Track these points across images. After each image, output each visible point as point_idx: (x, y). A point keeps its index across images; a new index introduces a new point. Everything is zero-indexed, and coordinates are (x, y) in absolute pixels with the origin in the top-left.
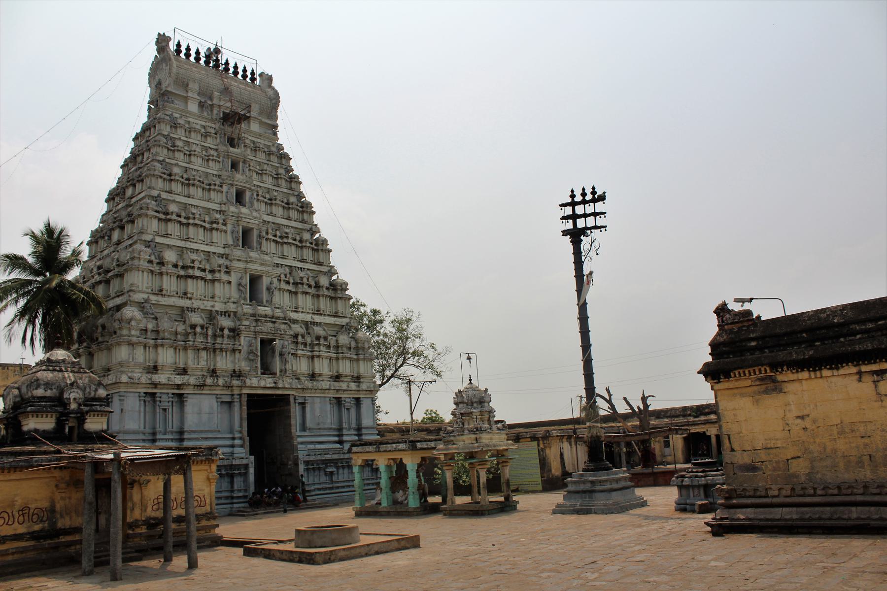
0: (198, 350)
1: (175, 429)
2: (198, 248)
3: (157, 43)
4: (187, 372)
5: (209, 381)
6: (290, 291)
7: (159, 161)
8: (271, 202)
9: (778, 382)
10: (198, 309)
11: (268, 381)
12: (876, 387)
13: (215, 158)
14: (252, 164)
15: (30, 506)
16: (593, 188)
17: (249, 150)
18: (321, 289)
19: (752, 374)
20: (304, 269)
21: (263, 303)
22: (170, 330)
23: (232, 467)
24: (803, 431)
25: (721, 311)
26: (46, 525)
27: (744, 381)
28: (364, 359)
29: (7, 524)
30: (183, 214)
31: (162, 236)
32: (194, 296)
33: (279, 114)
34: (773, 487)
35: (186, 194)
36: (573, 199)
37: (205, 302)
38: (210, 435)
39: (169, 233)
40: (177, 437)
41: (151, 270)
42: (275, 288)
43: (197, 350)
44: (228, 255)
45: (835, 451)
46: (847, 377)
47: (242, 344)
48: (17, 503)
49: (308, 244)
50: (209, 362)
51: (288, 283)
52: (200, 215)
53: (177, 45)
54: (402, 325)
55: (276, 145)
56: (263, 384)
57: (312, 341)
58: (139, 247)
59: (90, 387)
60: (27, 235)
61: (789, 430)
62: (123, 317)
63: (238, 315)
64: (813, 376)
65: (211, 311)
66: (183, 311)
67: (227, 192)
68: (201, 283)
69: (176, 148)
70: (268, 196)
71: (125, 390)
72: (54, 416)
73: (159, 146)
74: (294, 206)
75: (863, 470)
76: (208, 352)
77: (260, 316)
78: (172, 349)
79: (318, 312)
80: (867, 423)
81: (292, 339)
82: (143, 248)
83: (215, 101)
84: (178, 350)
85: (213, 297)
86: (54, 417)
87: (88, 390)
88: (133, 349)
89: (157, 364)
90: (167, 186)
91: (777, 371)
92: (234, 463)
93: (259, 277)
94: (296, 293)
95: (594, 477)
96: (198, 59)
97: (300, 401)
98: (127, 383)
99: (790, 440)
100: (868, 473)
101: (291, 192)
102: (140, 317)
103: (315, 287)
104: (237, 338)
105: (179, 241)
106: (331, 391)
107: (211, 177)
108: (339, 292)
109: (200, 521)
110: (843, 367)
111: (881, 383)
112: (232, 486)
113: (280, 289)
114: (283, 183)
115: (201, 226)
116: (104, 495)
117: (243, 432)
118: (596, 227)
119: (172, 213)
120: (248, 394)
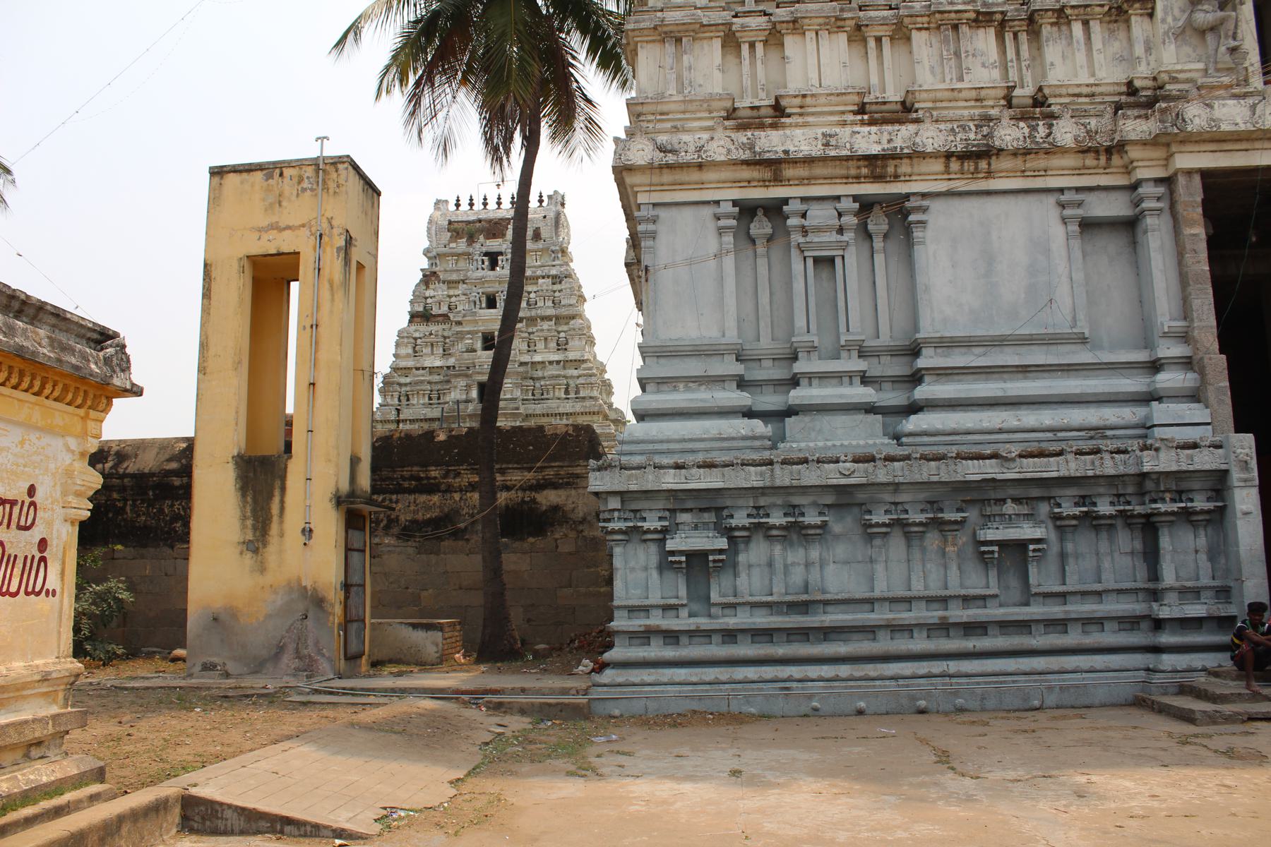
0: (955, 27)
1: (885, 339)
5: (1009, 134)
71: (656, 198)
76: (1009, 37)
84: (872, 43)
92: (1147, 468)
98: (650, 167)
112: (1154, 575)
120: (1206, 174)
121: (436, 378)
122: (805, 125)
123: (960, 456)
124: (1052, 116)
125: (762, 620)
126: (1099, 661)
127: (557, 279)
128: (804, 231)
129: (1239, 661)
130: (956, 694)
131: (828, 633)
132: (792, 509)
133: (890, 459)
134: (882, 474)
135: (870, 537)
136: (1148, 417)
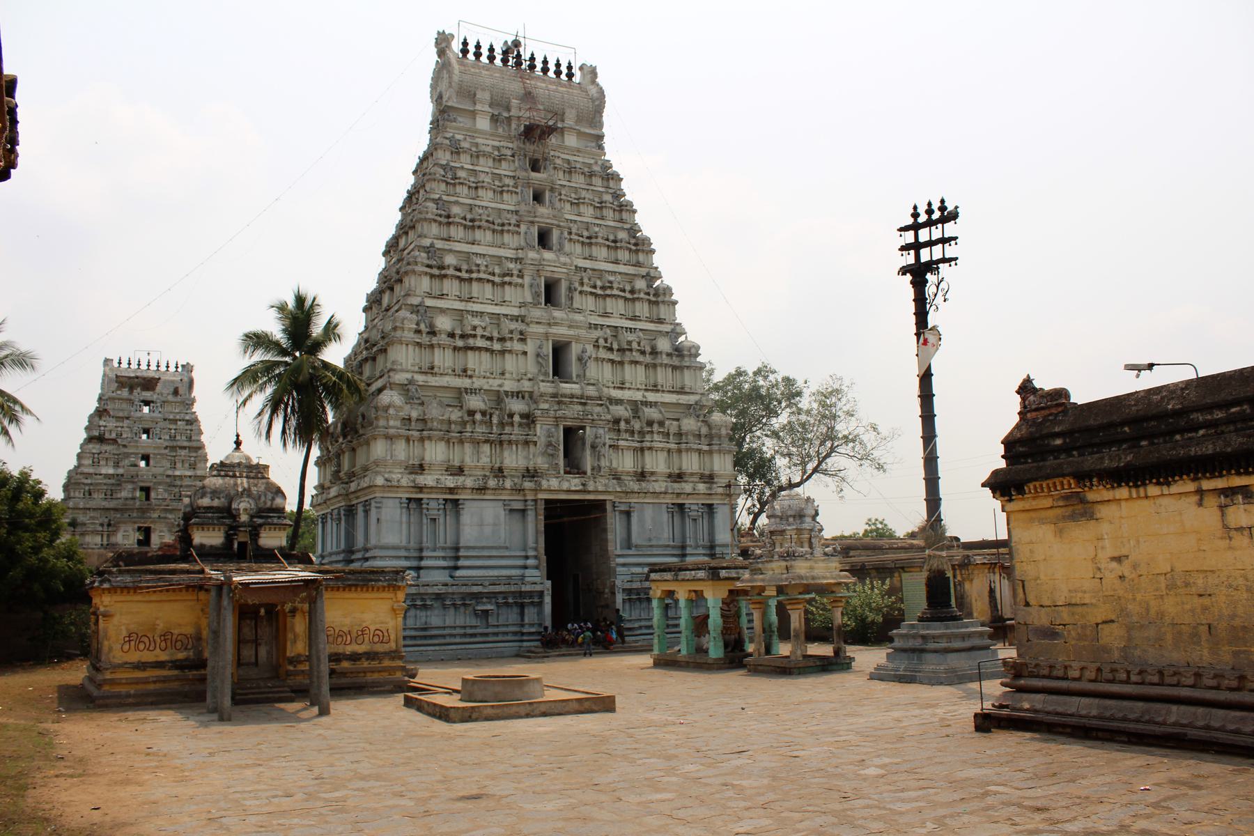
0: (478, 443)
1: (449, 544)
2: (483, 311)
3: (437, 43)
4: (463, 471)
5: (492, 483)
6: (612, 361)
7: (434, 200)
8: (589, 242)
9: (1088, 502)
10: (480, 390)
11: (574, 483)
12: (1223, 516)
13: (510, 188)
14: (563, 192)
15: (172, 631)
16: (942, 201)
17: (561, 173)
18: (659, 356)
19: (1052, 489)
20: (635, 329)
21: (572, 379)
22: (441, 418)
23: (521, 594)
24: (1119, 581)
25: (1026, 388)
26: (191, 653)
27: (1041, 500)
28: (720, 451)
29: (148, 649)
30: (465, 267)
31: (435, 297)
32: (477, 373)
33: (605, 119)
34: (1073, 664)
35: (470, 239)
36: (916, 220)
37: (491, 381)
38: (494, 553)
39: (444, 293)
40: (450, 554)
41: (418, 343)
42: (590, 358)
43: (476, 443)
44: (525, 316)
45: (1161, 615)
46: (1183, 498)
47: (538, 434)
48: (159, 628)
49: (642, 295)
50: (494, 459)
51: (611, 349)
52: (487, 266)
53: (463, 43)
54: (828, 397)
55: (600, 163)
56: (565, 486)
57: (642, 428)
58: (404, 313)
59: (265, 496)
60: (273, 307)
61: (1101, 579)
62: (379, 404)
63: (535, 397)
64: (1134, 495)
65: (499, 391)
66: (460, 393)
67: (526, 233)
68: (485, 356)
69: (457, 181)
70: (586, 234)
72: (222, 529)
73: (435, 180)
74: (623, 244)
75: (1198, 648)
76: (493, 445)
77: (564, 396)
78: (443, 442)
79: (655, 388)
80: (1208, 573)
81: (611, 425)
82: (408, 315)
83: (514, 112)
84: (451, 444)
85: (503, 374)
86: (222, 531)
87: (263, 499)
88: (392, 444)
89: (423, 462)
90: (444, 232)
91: (1085, 486)
92: (523, 590)
93: (567, 345)
94: (621, 363)
95: (928, 629)
96: (491, 58)
97: (623, 508)
98: (383, 486)
99: (1101, 594)
100: (1206, 652)
101: (619, 225)
102: (401, 404)
103: (651, 353)
104: (532, 426)
105: (458, 303)
106: (667, 496)
107: (505, 214)
108: (686, 359)
109: (381, 660)
110: (1175, 481)
111: (1231, 510)
112: (522, 620)
113: (597, 359)
114: (609, 213)
115: (488, 281)
116: (265, 623)
117: (539, 549)
118: (944, 260)
119: (449, 266)
121: (112, 481)
122: (431, 474)
123: (473, 585)
124: (504, 476)
125: (413, 633)
126: (507, 644)
128: (428, 509)
129: (542, 643)
130: (468, 654)
131: (432, 637)
132: (423, 600)
133: (453, 585)
134: (450, 590)
135: (444, 608)
136: (524, 574)
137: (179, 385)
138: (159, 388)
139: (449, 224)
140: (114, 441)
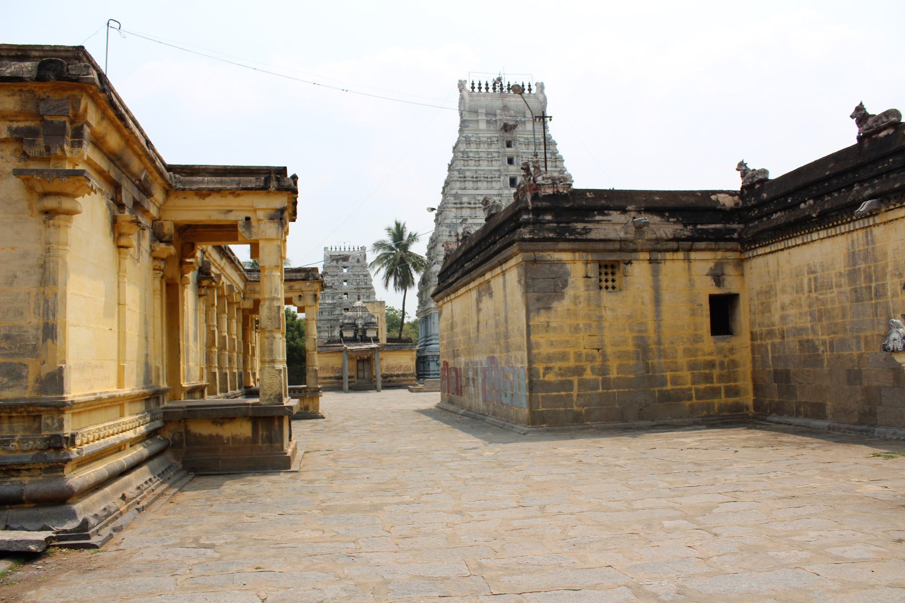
13: (496, 158)
14: (524, 156)
30: (473, 202)
35: (476, 187)
82: (445, 228)
83: (498, 117)
107: (493, 172)
121: (329, 306)
127: (365, 276)
137: (360, 258)
138: (350, 259)
139: (465, 181)
140: (331, 287)
